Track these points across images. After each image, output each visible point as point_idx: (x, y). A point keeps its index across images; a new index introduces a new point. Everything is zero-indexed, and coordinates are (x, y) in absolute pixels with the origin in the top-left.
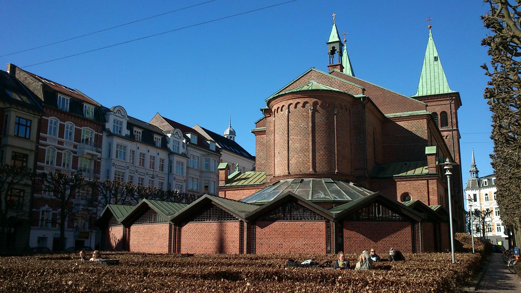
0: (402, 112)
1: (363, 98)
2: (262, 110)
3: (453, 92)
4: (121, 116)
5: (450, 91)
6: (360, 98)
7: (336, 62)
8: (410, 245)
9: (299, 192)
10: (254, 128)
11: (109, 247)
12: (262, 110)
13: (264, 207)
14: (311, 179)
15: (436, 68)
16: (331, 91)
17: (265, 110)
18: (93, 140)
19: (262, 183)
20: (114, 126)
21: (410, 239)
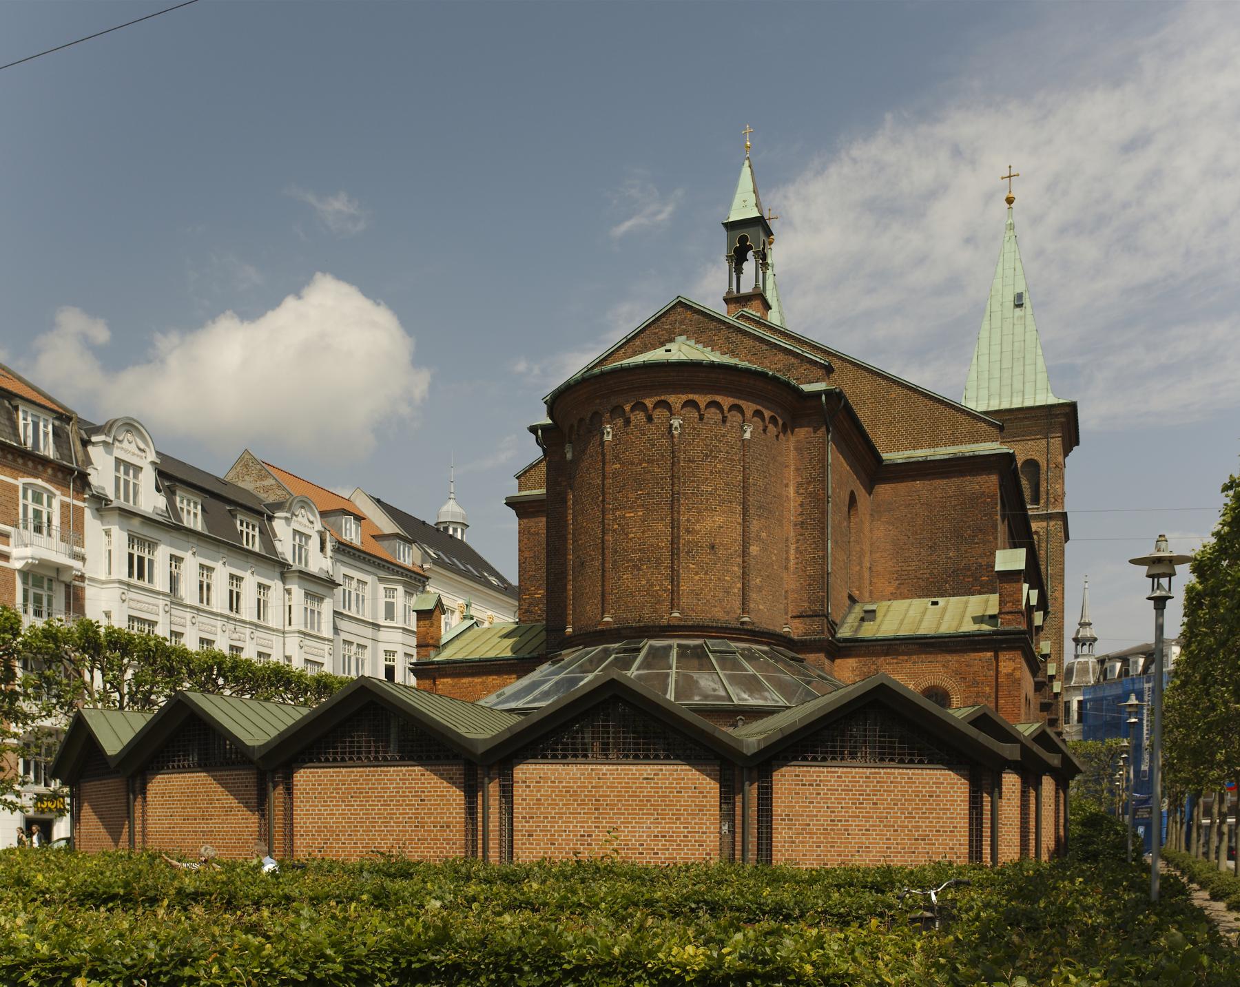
0: (929, 446)
1: (828, 393)
2: (533, 429)
3: (1061, 401)
4: (137, 451)
5: (1052, 400)
6: (817, 395)
7: (747, 287)
8: (965, 840)
9: (639, 677)
10: (513, 489)
11: (1095, 844)
12: (533, 429)
13: (535, 718)
14: (675, 642)
15: (1019, 329)
16: (734, 368)
17: (544, 428)
18: (56, 521)
19: (535, 654)
20: (117, 479)
21: (964, 823)
